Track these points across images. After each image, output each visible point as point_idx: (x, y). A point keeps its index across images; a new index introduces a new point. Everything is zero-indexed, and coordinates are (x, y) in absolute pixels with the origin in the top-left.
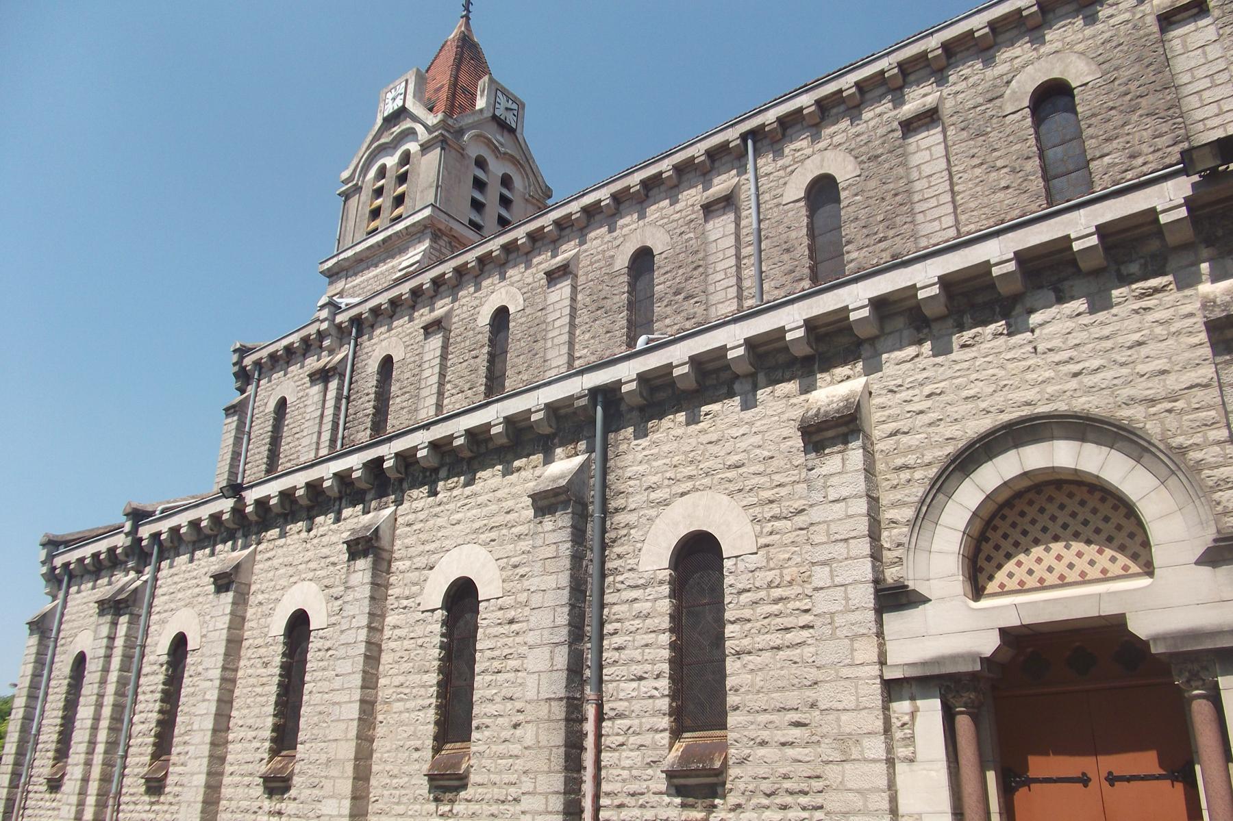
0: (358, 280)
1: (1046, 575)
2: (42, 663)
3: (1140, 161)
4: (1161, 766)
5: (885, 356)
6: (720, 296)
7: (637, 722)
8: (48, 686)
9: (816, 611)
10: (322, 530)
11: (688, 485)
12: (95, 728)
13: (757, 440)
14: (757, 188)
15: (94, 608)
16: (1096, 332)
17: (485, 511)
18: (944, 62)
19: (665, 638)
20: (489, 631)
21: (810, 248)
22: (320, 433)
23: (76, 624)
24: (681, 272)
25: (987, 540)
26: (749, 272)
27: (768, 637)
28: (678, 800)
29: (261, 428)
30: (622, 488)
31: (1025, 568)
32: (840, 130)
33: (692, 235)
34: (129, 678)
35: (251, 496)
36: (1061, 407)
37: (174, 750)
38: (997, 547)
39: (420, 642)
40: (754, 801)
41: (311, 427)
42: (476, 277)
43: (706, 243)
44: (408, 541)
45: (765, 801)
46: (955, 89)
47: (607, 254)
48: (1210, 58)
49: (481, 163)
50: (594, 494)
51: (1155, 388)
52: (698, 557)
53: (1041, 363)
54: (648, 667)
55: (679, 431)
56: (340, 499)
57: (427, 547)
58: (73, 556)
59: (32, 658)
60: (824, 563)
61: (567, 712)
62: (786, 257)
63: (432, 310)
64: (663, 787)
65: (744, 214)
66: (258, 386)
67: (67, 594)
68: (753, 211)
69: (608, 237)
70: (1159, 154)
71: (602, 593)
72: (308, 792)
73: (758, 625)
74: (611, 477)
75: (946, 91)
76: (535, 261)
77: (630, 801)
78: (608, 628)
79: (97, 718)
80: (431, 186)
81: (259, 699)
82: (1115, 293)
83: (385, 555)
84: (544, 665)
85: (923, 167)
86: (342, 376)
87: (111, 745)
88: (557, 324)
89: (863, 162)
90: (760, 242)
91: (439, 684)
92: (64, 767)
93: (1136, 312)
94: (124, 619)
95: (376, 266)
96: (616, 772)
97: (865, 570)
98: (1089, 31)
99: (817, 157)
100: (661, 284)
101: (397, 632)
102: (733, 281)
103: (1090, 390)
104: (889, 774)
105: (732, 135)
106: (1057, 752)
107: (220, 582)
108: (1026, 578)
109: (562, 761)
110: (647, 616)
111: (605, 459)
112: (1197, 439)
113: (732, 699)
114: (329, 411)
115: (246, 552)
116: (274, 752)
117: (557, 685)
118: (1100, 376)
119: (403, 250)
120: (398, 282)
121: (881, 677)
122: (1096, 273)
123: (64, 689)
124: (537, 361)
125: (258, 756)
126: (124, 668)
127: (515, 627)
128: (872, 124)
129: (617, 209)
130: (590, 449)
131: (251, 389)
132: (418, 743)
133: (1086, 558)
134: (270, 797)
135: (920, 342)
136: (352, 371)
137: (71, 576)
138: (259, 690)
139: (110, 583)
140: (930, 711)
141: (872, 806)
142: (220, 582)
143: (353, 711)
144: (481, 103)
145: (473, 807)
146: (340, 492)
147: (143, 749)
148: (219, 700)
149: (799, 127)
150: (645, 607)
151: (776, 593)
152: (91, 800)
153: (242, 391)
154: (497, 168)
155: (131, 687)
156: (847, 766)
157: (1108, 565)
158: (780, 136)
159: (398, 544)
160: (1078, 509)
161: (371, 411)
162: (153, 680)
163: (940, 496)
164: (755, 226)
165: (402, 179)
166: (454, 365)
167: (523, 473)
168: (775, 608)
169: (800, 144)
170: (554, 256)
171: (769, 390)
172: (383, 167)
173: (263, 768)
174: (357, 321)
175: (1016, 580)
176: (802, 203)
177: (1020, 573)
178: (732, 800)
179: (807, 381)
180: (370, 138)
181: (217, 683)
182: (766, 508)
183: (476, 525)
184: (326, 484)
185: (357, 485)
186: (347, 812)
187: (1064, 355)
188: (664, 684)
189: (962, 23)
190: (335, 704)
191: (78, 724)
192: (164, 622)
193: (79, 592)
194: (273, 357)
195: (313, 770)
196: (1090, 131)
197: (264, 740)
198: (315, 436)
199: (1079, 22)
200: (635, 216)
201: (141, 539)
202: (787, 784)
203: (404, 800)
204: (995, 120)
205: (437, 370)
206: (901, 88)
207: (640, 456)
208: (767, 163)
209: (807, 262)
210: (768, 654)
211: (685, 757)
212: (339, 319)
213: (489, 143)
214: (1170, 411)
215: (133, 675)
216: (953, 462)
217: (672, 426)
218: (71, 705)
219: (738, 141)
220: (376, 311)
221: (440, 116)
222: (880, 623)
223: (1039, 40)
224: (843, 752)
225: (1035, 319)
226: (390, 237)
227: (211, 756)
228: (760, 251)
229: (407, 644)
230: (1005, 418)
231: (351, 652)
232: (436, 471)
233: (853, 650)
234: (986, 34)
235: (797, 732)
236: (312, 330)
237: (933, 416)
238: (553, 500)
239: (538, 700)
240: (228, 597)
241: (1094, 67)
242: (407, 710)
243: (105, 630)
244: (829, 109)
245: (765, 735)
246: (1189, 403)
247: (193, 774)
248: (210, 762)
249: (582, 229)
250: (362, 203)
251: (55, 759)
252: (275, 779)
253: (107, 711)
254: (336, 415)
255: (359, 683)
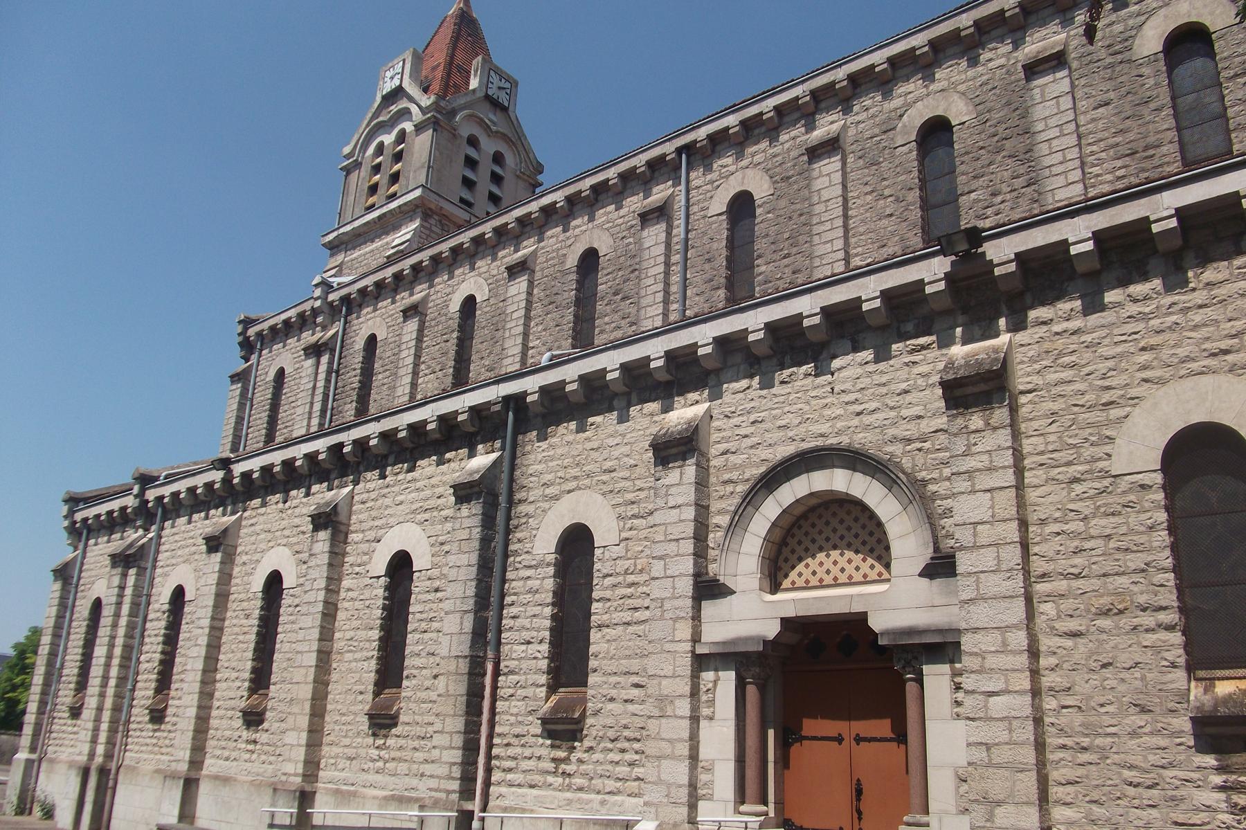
0: (356, 253)
1: (825, 577)
2: (65, 606)
3: (999, 199)
4: (893, 731)
5: (725, 386)
6: (649, 300)
7: (523, 677)
8: (70, 626)
9: (652, 596)
10: (295, 502)
11: (573, 484)
12: (108, 665)
13: (626, 449)
14: (688, 200)
15: (107, 561)
16: (878, 379)
17: (422, 495)
18: (849, 92)
19: (548, 611)
20: (420, 597)
21: (728, 259)
22: (312, 403)
23: (93, 573)
24: (620, 273)
25: (787, 545)
26: (676, 278)
27: (621, 614)
28: (549, 742)
29: (263, 396)
30: (525, 482)
31: (810, 570)
32: (759, 150)
33: (631, 240)
34: (136, 623)
35: (238, 469)
36: (845, 440)
37: (173, 686)
38: (793, 552)
39: (367, 603)
40: (602, 745)
41: (304, 397)
42: (450, 266)
43: (641, 250)
44: (362, 517)
45: (610, 745)
46: (858, 118)
47: (561, 252)
48: (1062, 109)
49: (473, 142)
50: (503, 488)
51: (911, 430)
52: (576, 543)
53: (836, 402)
54: (534, 634)
55: (570, 438)
56: (310, 476)
57: (377, 523)
58: (91, 512)
59: (56, 602)
60: (660, 558)
61: (470, 668)
62: (707, 266)
63: (412, 295)
64: (539, 731)
65: (676, 223)
66: (260, 356)
67: (86, 545)
68: (682, 222)
69: (562, 237)
70: (1015, 194)
71: (504, 571)
72: (278, 725)
73: (615, 604)
74: (517, 473)
75: (850, 120)
76: (500, 254)
77: (513, 741)
78: (508, 600)
79: (109, 657)
80: (423, 167)
81: (241, 645)
82: (894, 347)
83: (343, 528)
84: (455, 629)
85: (823, 192)
86: (333, 351)
87: (122, 680)
88: (515, 315)
89: (776, 182)
90: (686, 251)
91: (380, 639)
92: (83, 698)
93: (907, 364)
94: (132, 571)
95: (373, 241)
96: (506, 717)
97: (688, 565)
98: (971, 73)
99: (739, 175)
100: (604, 285)
101: (350, 594)
102: (661, 286)
103: (867, 428)
104: (691, 729)
105: (669, 148)
106: (825, 716)
107: (211, 544)
108: (854, 573)
109: (464, 707)
110: (537, 591)
111: (513, 457)
112: (935, 475)
113: (593, 663)
114: (321, 384)
115: (234, 518)
116: (253, 691)
117: (463, 646)
118: (875, 416)
119: (396, 228)
120: (391, 261)
121: (693, 652)
122: (883, 328)
123: (83, 629)
124: (497, 349)
125: (240, 693)
126: (133, 614)
127: (439, 595)
128: (787, 146)
129: (571, 210)
130: (503, 448)
131: (254, 358)
132: (362, 688)
133: (854, 565)
134: (248, 729)
135: (751, 377)
136: (342, 347)
137: (90, 530)
138: (241, 638)
139: (122, 538)
140: (728, 679)
141: (677, 753)
142: (211, 544)
143: (311, 659)
144: (474, 83)
145: (402, 742)
146: (310, 470)
147: (148, 684)
148: (209, 646)
149: (726, 144)
150: (534, 584)
151: (630, 578)
152: (104, 726)
153: (247, 360)
154: (489, 146)
155: (138, 631)
156: (663, 720)
157: (868, 571)
158: (709, 152)
159: (354, 517)
160: (852, 524)
161: (356, 385)
162: (156, 626)
163: (749, 508)
164: (682, 236)
165: (398, 157)
166: (428, 347)
167: (452, 464)
168: (629, 591)
169: (726, 161)
170: (516, 251)
171: (638, 407)
172: (381, 145)
173: (243, 704)
174: (346, 300)
175: (803, 578)
176: (724, 217)
177: (807, 573)
178: (587, 743)
179: (667, 402)
180: (370, 115)
181: (207, 631)
182: (629, 508)
183: (414, 507)
184: (298, 463)
185: (323, 465)
186: (304, 742)
187: (851, 397)
188: (545, 647)
189: (866, 58)
190: (298, 652)
191: (94, 661)
192: (166, 575)
193: (96, 544)
194: (273, 329)
195: (282, 707)
196: (962, 168)
197: (244, 680)
198: (308, 406)
199: (964, 64)
200: (586, 218)
201: (148, 502)
202: (626, 733)
203: (350, 734)
204: (887, 151)
205: (412, 351)
206: (813, 114)
207: (540, 457)
208: (698, 177)
209: (723, 272)
210: (621, 628)
211: (555, 709)
212: (331, 297)
213: (481, 122)
214: (920, 450)
215: (140, 620)
216: (760, 480)
217: (565, 432)
218: (89, 644)
219: (673, 155)
220: (363, 292)
221: (433, 98)
222: (697, 609)
223: (929, 78)
224: (661, 709)
225: (836, 363)
226: (384, 214)
227: (201, 693)
228: (686, 259)
229: (358, 604)
230: (805, 446)
231: (313, 610)
232: (385, 457)
233: (674, 630)
234: (885, 70)
235: (636, 692)
236: (307, 306)
237: (754, 440)
238: (469, 491)
239: (449, 657)
240: (217, 557)
241: (971, 108)
242: (356, 660)
243: (116, 581)
244: (752, 130)
245: (614, 693)
246: (933, 445)
247: (186, 707)
248: (200, 698)
249: (541, 227)
250: (361, 179)
251: (76, 690)
252: (251, 713)
253: (118, 651)
254: (327, 388)
255: (317, 636)
